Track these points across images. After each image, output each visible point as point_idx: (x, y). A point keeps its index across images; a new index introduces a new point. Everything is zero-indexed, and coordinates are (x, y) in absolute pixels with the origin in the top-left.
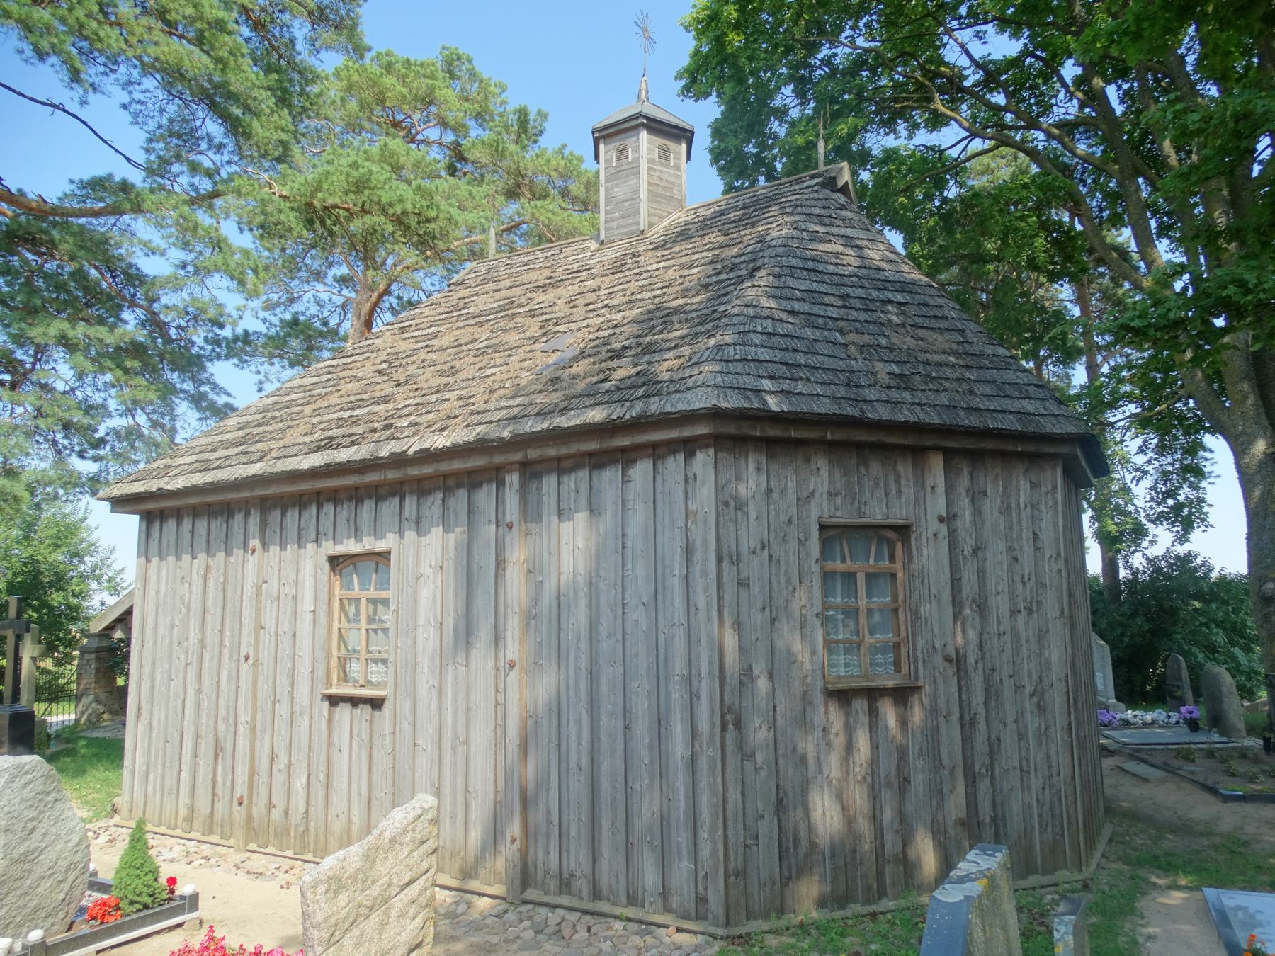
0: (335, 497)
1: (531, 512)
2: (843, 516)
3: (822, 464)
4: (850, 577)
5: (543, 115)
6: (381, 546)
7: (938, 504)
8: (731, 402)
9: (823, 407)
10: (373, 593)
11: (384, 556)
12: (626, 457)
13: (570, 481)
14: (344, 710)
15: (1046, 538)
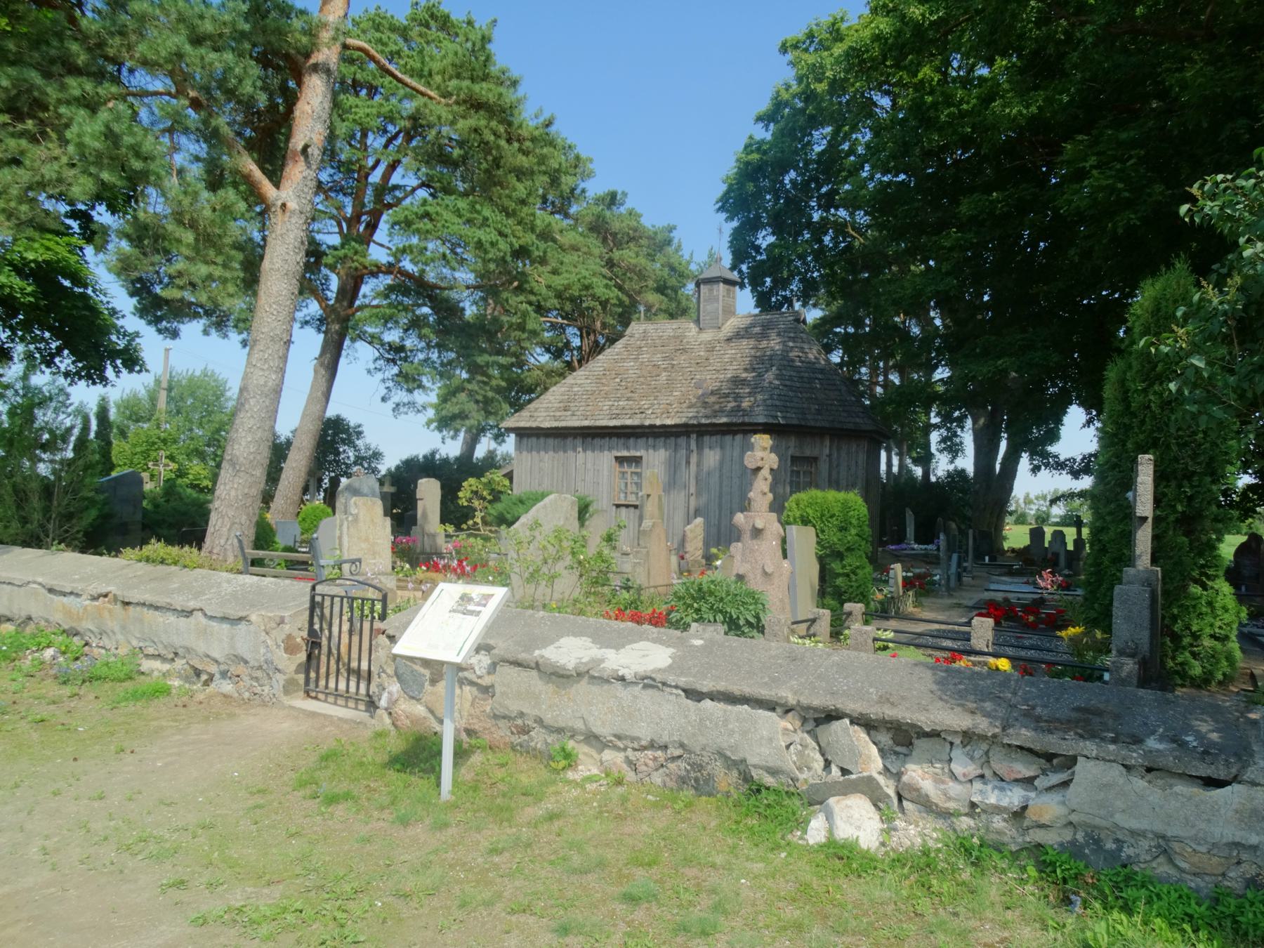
0: (619, 436)
1: (700, 448)
2: (798, 454)
3: (793, 439)
4: (798, 472)
5: (625, 194)
6: (638, 454)
7: (827, 451)
8: (771, 421)
9: (795, 422)
10: (633, 469)
11: (641, 458)
12: (735, 433)
13: (714, 438)
14: (623, 510)
15: (860, 463)
